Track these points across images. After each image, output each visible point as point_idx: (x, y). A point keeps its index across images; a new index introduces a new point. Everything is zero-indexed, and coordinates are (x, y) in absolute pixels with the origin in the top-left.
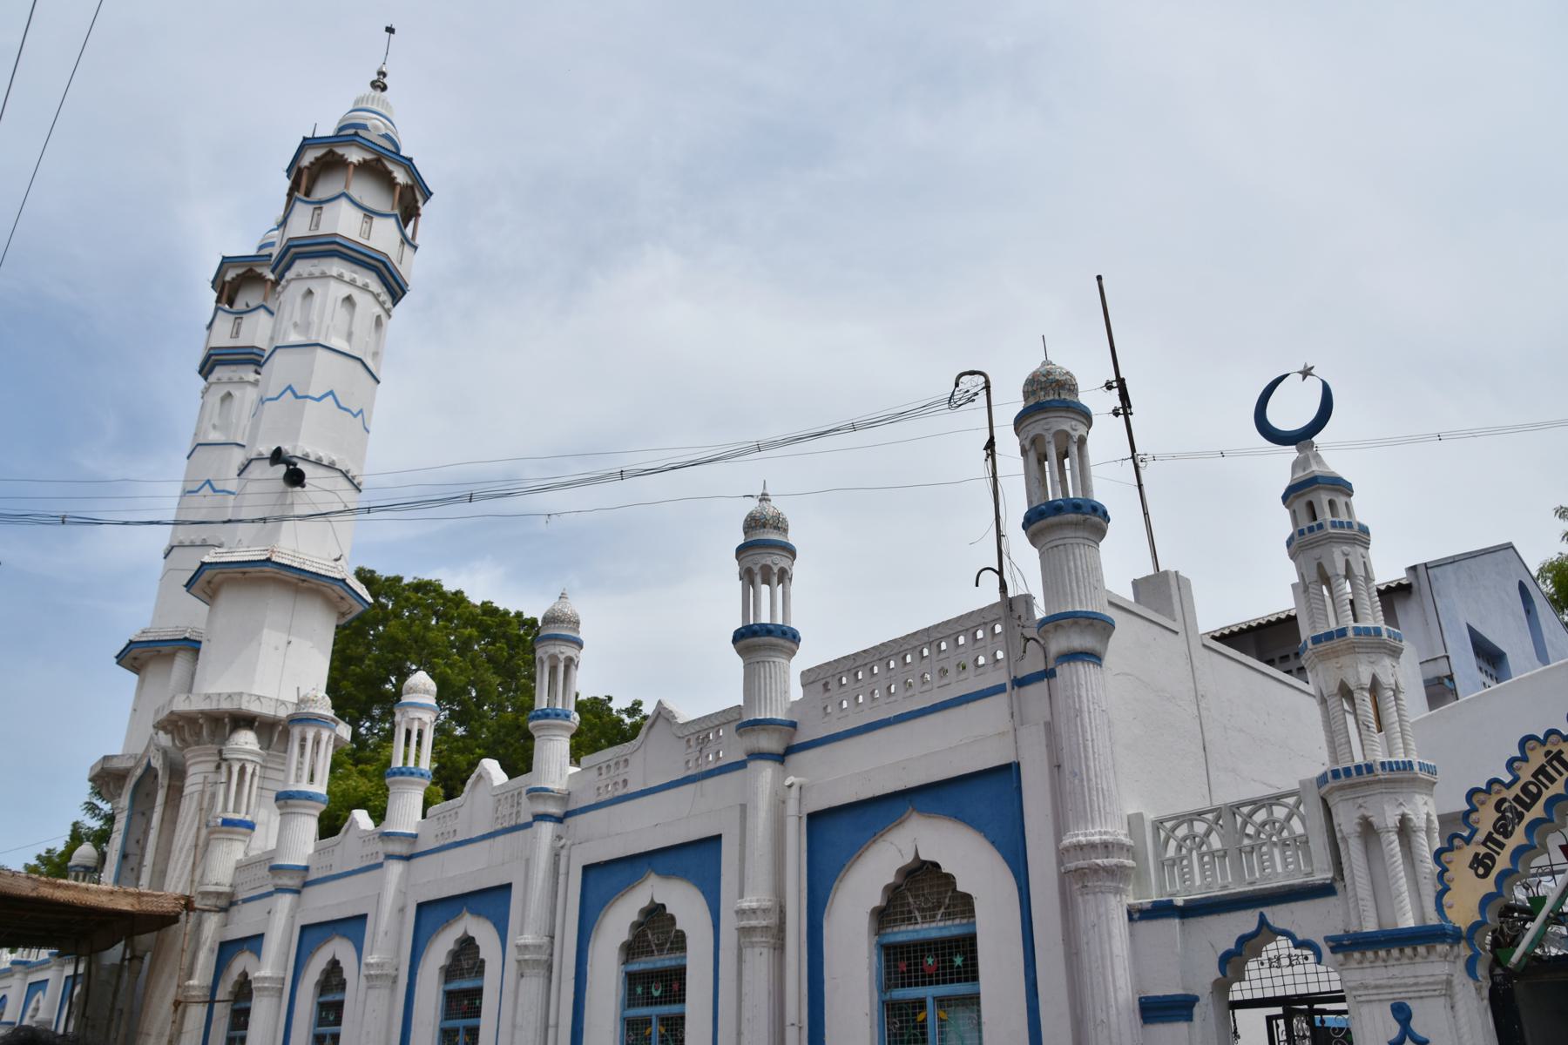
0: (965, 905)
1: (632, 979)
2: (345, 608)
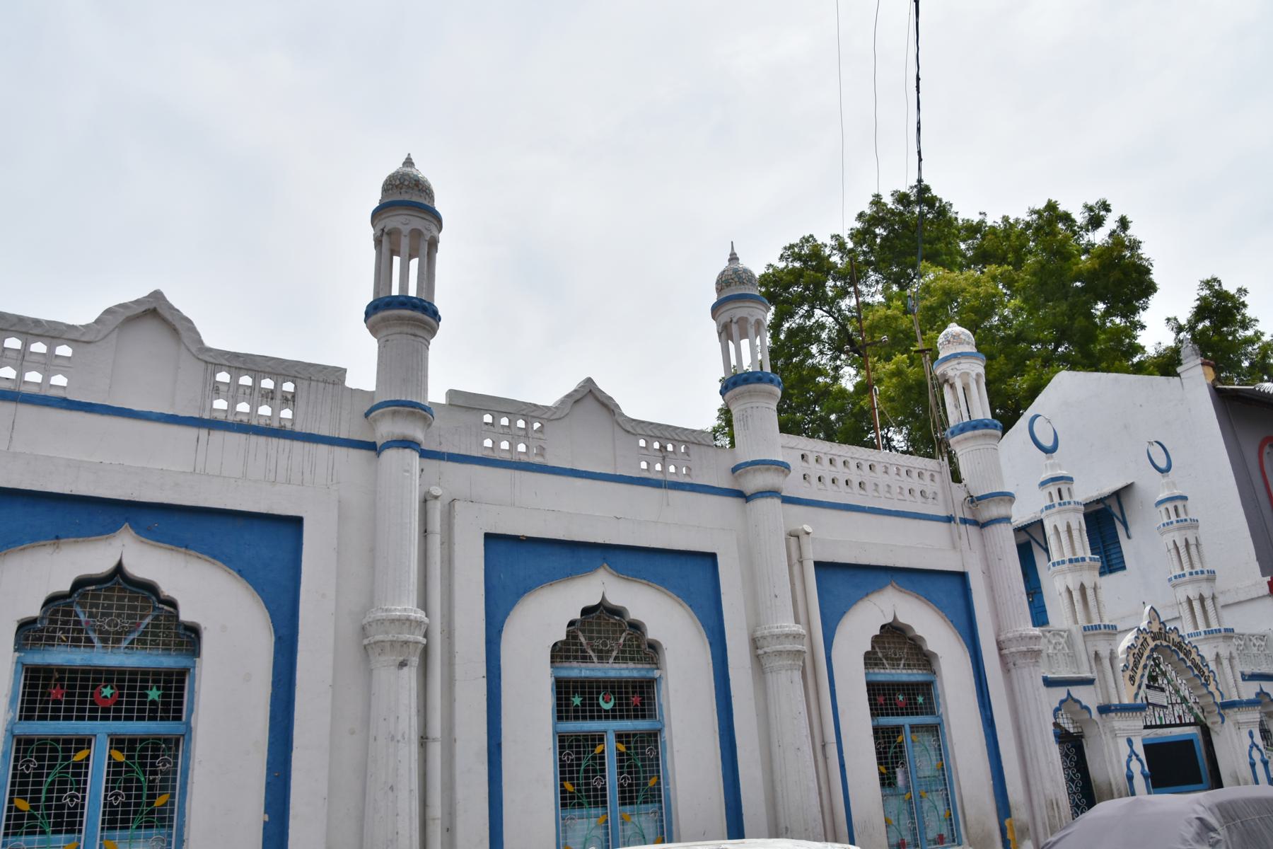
0: (651, 652)
1: (563, 689)
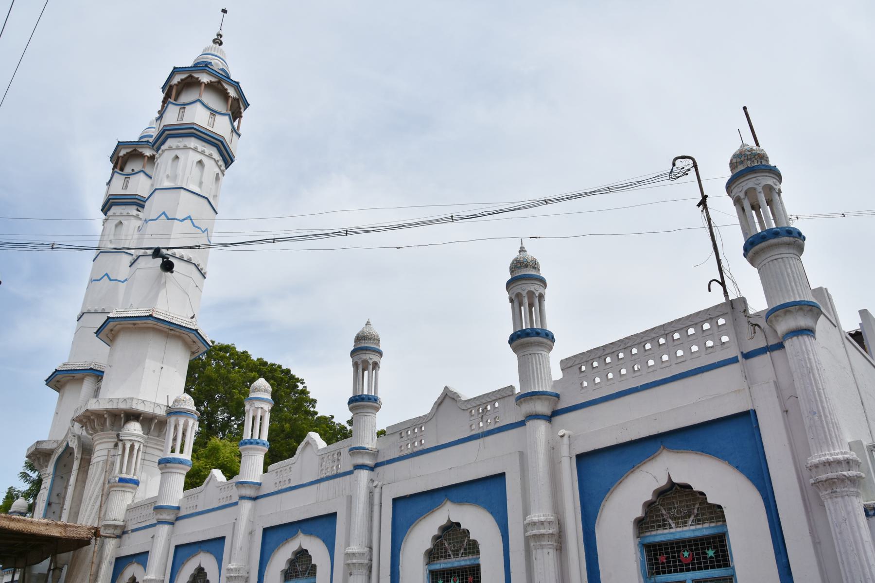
0: (473, 548)
2: (195, 348)
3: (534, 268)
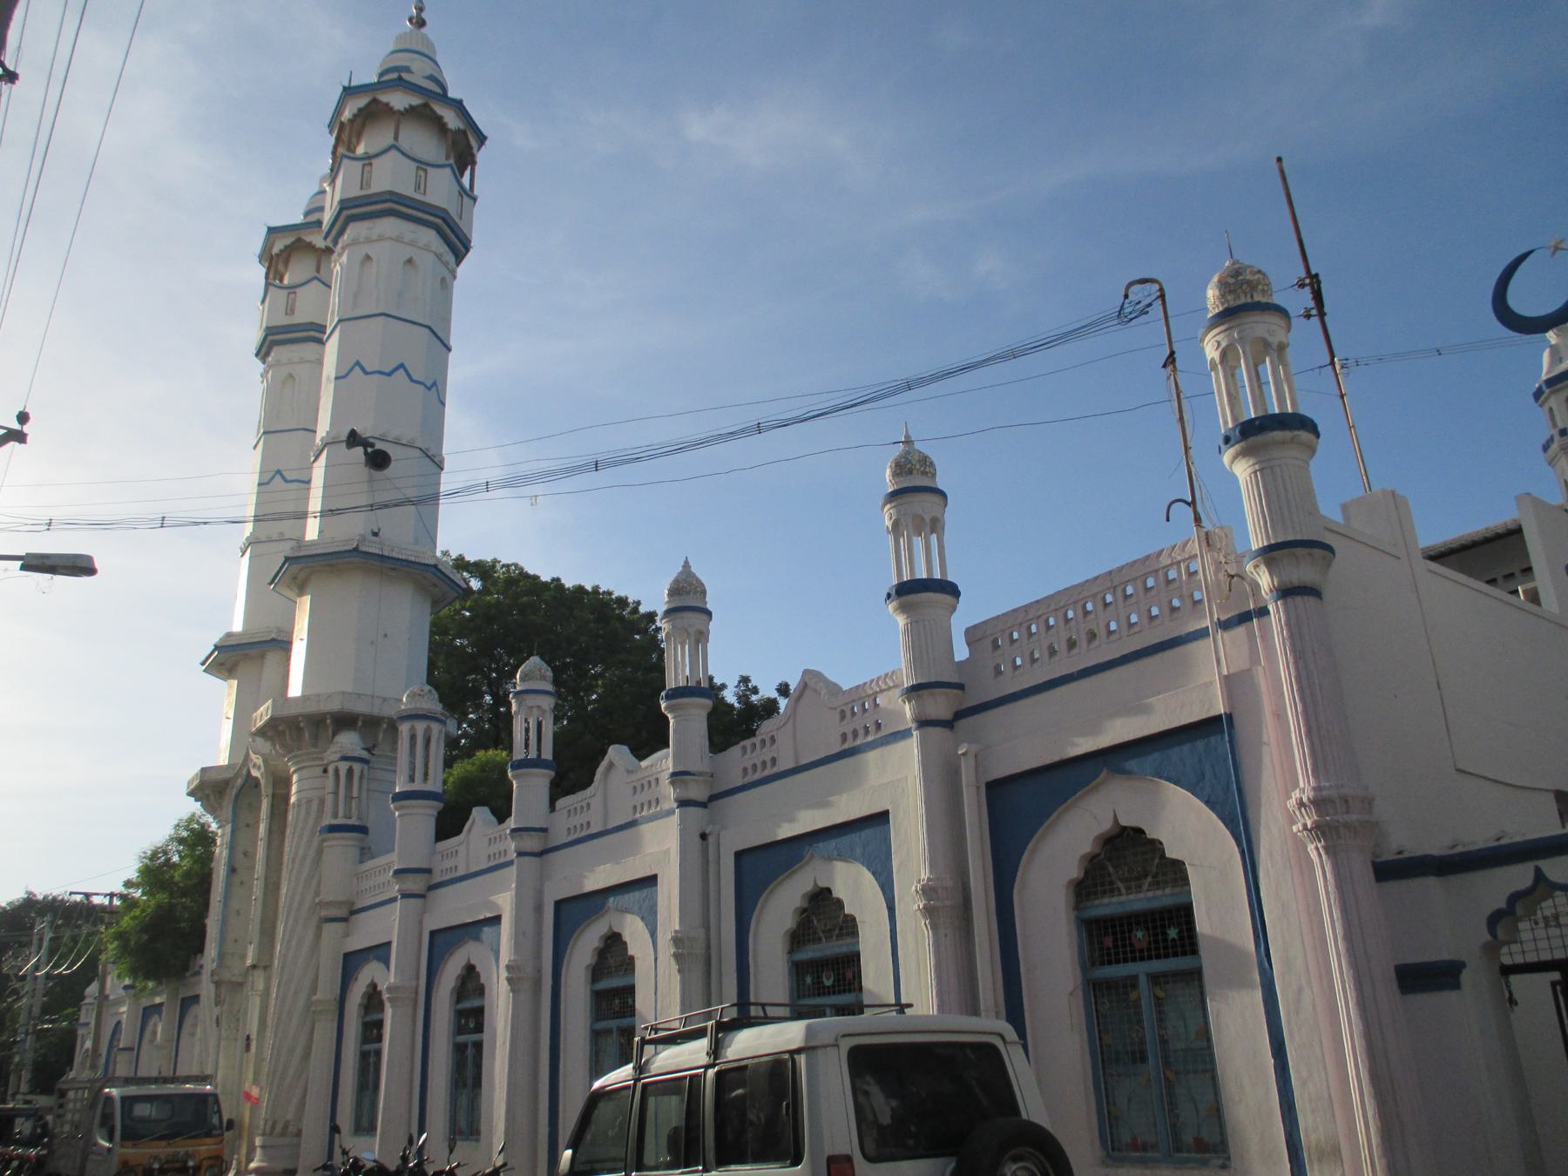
0: (849, 927)
3: (924, 473)
